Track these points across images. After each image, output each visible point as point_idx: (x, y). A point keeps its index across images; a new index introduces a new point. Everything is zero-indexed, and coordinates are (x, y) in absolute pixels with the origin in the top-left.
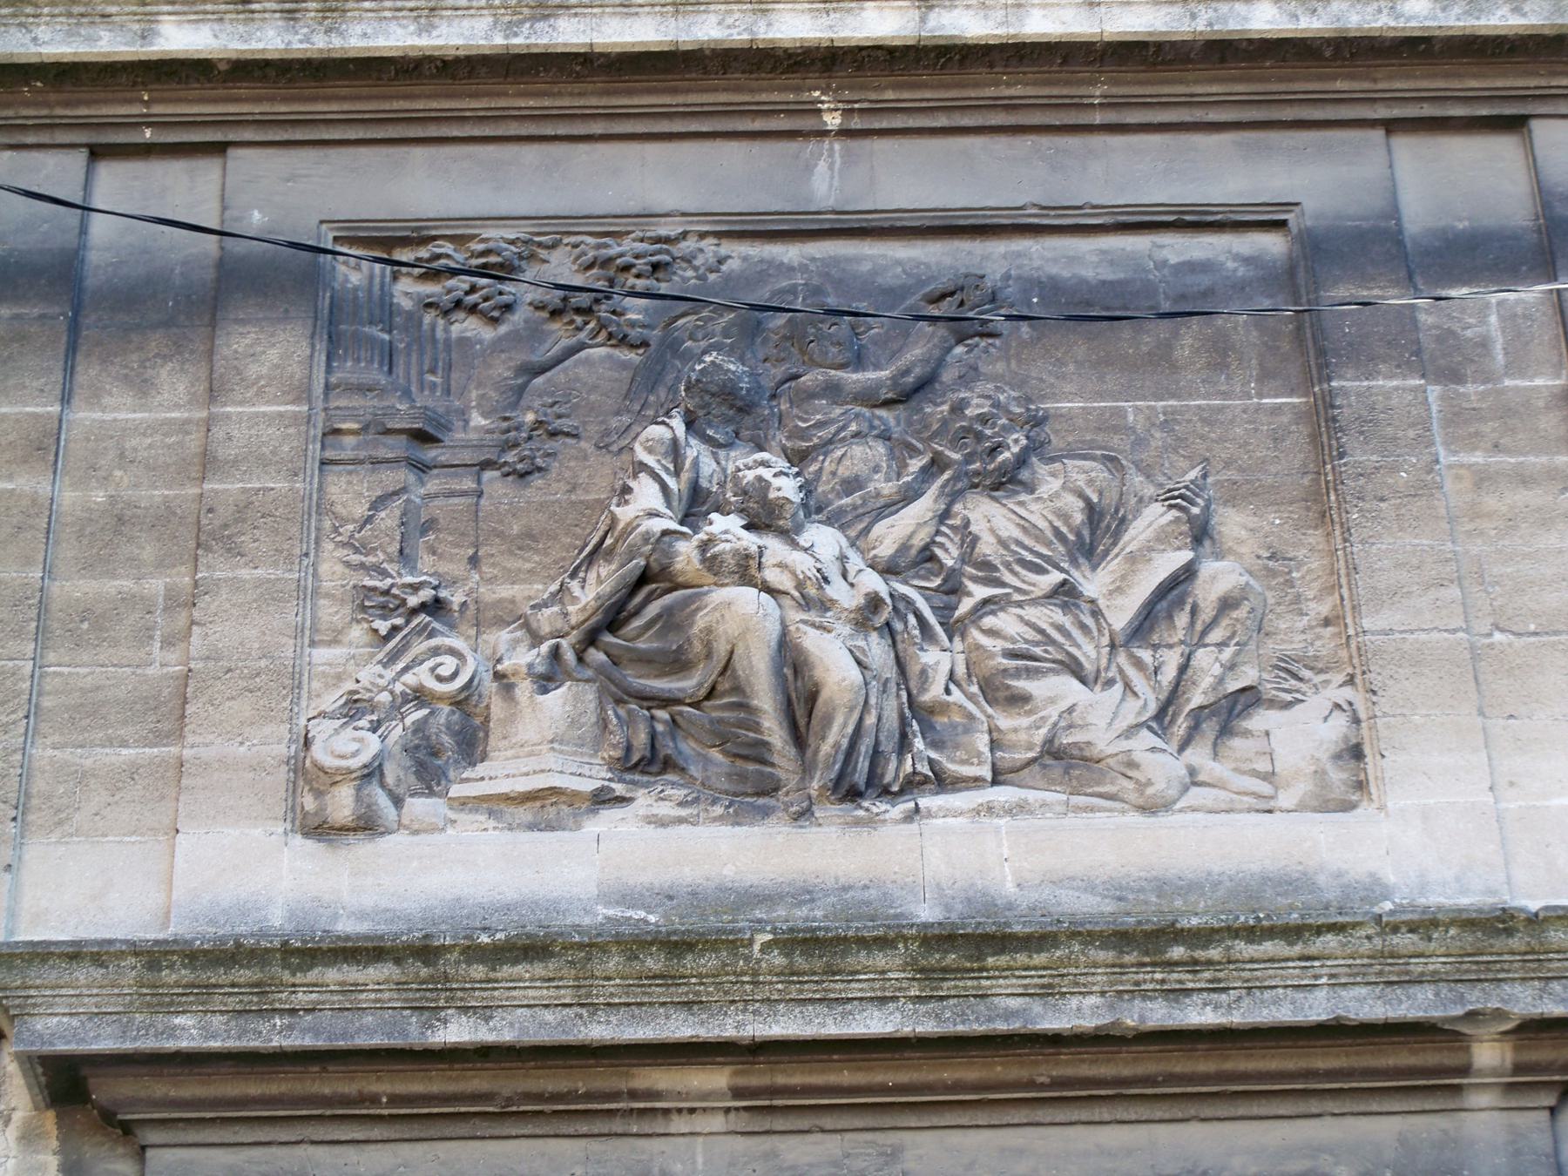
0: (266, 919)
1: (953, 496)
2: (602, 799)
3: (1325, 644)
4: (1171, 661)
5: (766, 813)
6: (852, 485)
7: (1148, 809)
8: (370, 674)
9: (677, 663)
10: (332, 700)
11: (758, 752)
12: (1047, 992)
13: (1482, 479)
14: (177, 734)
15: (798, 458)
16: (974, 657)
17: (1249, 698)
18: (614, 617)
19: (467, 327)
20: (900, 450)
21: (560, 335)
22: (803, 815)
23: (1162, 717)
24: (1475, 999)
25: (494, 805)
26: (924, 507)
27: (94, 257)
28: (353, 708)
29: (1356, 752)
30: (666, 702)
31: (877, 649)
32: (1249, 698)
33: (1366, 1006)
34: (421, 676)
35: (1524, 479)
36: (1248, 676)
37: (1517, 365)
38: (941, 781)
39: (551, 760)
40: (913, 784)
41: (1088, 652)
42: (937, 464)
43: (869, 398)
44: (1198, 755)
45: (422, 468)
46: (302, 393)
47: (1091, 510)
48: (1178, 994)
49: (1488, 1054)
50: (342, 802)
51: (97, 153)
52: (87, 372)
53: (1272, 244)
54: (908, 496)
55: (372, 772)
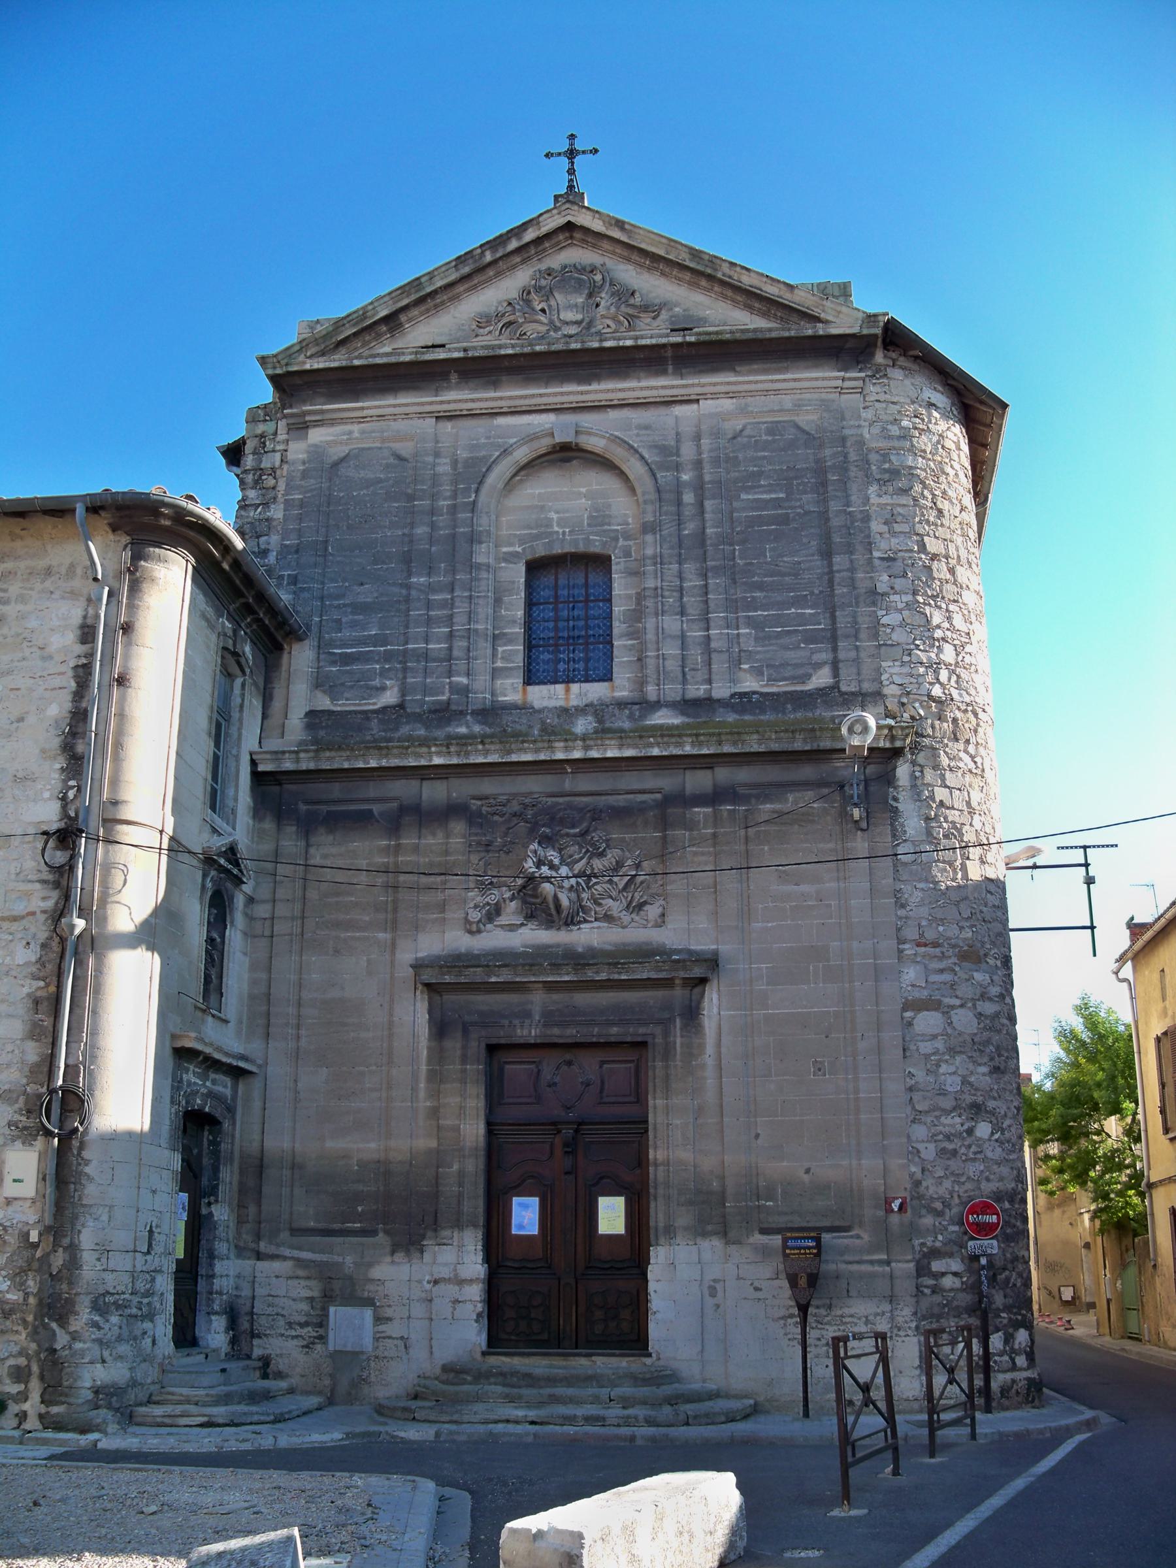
0: (609, 506)
1: (590, 858)
2: (522, 925)
3: (660, 891)
4: (630, 895)
5: (552, 927)
6: (571, 856)
7: (624, 927)
8: (479, 899)
9: (536, 896)
10: (472, 905)
11: (551, 915)
12: (597, 973)
13: (695, 854)
14: (443, 911)
15: (560, 850)
16: (593, 894)
17: (645, 903)
18: (524, 887)
19: (496, 818)
20: (581, 847)
21: (515, 820)
22: (559, 929)
23: (628, 907)
24: (673, 974)
25: (502, 926)
26: (584, 861)
27: (423, 804)
28: (476, 907)
29: (663, 915)
30: (534, 904)
31: (573, 895)
32: (645, 903)
33: (653, 975)
34: (488, 899)
35: (703, 854)
36: (645, 898)
37: (705, 828)
38: (586, 921)
39: (512, 917)
40: (580, 922)
41: (614, 894)
42: (588, 851)
43: (575, 835)
44: (633, 916)
45: (488, 851)
46: (464, 837)
47: (617, 862)
48: (620, 973)
49: (677, 981)
50: (474, 928)
51: (422, 779)
52: (424, 831)
53: (658, 796)
54: (582, 859)
55: (480, 921)
